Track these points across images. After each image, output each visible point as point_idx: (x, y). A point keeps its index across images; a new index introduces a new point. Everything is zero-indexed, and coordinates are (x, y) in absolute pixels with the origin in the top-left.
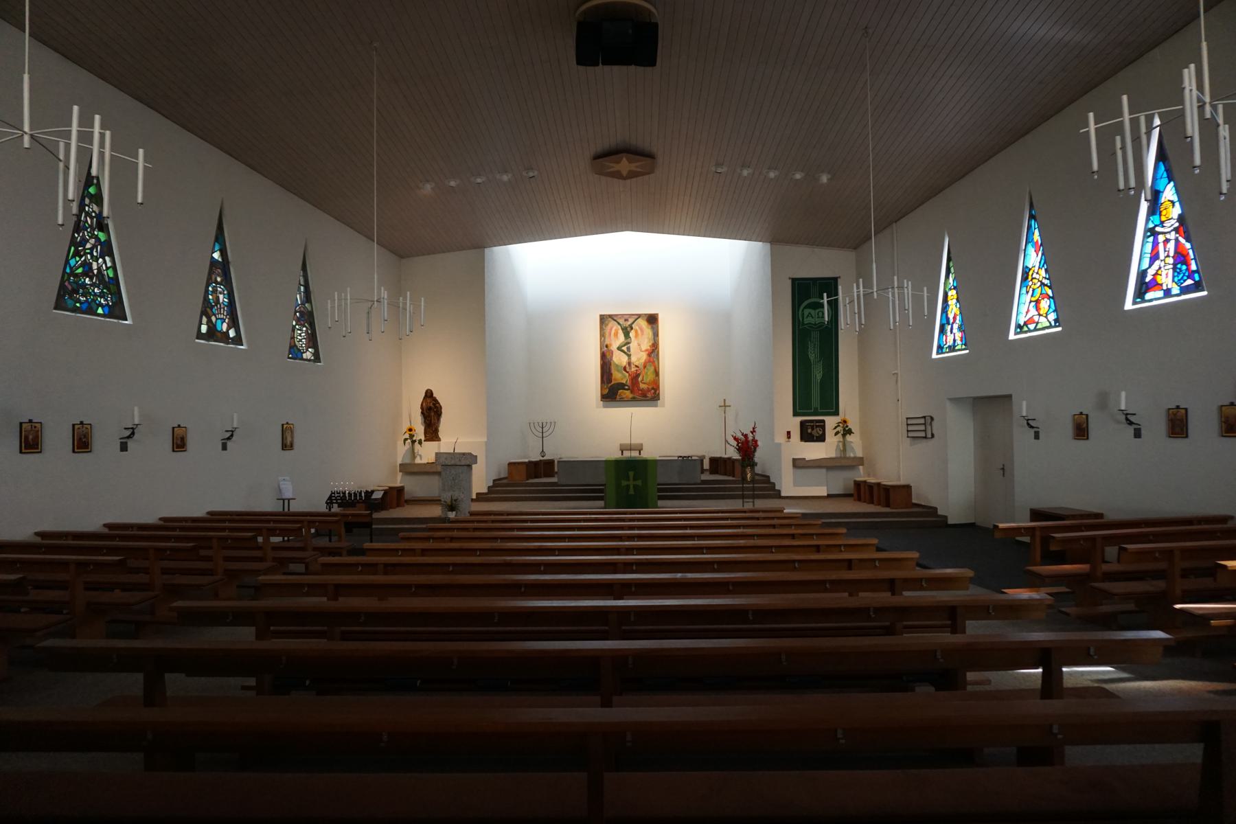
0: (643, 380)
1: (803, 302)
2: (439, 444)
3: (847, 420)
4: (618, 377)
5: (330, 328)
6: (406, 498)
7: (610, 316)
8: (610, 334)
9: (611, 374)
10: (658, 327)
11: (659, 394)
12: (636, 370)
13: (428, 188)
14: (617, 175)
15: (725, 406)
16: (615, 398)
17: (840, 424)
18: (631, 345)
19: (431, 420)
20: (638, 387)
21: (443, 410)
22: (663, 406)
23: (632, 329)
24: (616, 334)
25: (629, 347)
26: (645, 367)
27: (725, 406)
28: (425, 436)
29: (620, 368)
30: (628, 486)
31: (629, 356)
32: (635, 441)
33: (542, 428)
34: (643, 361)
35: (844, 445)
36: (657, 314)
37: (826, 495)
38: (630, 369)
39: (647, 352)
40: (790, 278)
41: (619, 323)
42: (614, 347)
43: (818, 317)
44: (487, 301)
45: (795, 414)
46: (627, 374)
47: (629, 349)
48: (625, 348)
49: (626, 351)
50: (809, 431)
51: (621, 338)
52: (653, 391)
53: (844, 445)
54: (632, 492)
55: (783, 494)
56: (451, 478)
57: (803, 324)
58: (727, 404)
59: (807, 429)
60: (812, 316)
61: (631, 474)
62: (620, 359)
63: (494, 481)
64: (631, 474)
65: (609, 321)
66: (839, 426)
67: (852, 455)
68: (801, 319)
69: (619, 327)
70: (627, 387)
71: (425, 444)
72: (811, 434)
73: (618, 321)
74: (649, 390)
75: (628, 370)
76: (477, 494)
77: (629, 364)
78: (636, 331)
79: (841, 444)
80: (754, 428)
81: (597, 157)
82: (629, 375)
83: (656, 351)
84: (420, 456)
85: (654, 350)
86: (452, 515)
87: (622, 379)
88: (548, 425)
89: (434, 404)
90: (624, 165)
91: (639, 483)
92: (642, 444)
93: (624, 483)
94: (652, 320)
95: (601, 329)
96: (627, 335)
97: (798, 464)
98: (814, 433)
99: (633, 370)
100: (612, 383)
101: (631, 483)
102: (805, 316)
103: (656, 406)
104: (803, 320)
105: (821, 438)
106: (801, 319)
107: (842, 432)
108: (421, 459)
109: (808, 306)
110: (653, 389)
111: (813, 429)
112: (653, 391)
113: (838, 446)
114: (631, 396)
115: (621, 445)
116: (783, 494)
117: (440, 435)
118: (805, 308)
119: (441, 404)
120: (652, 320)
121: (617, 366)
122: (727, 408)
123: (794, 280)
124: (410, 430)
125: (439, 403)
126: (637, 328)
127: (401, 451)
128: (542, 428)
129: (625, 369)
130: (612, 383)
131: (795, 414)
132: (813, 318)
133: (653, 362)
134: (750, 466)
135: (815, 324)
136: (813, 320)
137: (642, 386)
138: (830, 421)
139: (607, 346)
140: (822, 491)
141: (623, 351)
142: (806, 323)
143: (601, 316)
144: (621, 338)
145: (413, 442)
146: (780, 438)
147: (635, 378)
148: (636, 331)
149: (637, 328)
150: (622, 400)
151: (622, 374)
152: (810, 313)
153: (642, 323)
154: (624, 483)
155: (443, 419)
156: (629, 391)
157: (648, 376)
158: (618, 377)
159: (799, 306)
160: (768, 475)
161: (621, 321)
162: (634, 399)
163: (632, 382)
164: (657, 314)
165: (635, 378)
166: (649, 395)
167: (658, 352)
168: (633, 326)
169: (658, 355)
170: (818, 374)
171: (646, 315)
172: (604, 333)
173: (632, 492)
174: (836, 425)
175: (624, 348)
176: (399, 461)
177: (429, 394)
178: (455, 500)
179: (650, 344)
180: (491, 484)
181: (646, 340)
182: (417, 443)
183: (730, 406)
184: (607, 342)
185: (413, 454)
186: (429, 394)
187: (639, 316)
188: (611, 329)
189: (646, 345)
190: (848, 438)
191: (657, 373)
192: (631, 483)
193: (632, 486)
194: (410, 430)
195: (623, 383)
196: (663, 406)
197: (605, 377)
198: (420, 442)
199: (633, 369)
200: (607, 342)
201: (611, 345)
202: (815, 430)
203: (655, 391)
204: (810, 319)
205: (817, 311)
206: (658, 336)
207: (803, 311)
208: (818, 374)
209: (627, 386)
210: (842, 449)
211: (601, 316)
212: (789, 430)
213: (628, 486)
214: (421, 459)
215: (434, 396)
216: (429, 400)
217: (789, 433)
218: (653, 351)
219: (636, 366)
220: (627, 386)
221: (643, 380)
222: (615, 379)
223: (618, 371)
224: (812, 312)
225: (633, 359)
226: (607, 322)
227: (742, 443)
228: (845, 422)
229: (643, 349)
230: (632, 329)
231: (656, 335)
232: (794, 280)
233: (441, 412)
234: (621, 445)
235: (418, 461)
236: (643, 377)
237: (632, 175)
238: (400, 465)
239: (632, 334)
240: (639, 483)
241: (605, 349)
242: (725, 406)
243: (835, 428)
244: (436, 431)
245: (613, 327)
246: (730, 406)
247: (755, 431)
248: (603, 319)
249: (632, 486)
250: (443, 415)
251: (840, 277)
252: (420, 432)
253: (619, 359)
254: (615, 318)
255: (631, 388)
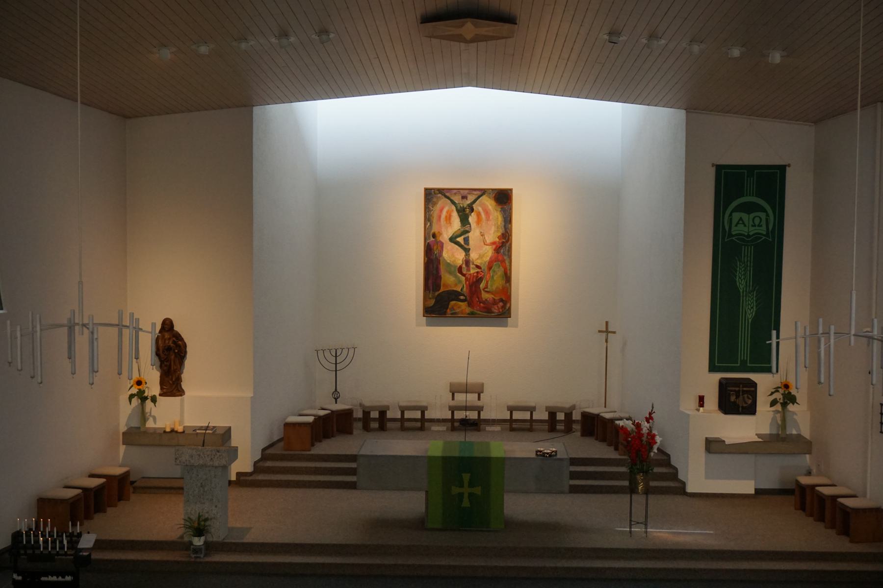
0: (486, 287)
1: (731, 203)
2: (182, 402)
3: (790, 385)
4: (450, 281)
5: (10, 363)
6: (131, 480)
7: (441, 191)
8: (440, 217)
9: (440, 277)
10: (511, 209)
11: (510, 308)
12: (477, 272)
13: (167, 54)
14: (460, 39)
15: (607, 331)
16: (445, 313)
17: (780, 390)
18: (470, 235)
19: (170, 365)
20: (479, 297)
21: (188, 349)
22: (516, 326)
23: (472, 210)
24: (449, 218)
25: (468, 237)
26: (490, 268)
27: (607, 331)
28: (162, 388)
29: (453, 269)
30: (461, 495)
31: (467, 251)
32: (473, 379)
33: (336, 356)
34: (487, 259)
35: (784, 420)
36: (511, 190)
37: (752, 491)
38: (469, 270)
39: (494, 246)
40: (713, 165)
41: (453, 202)
42: (445, 236)
43: (754, 226)
44: (256, 197)
45: (713, 368)
46: (463, 278)
47: (466, 240)
48: (461, 240)
49: (462, 243)
50: (733, 398)
51: (456, 224)
52: (501, 304)
53: (784, 420)
54: (466, 503)
55: (690, 489)
56: (199, 485)
57: (730, 235)
58: (610, 330)
59: (729, 395)
60: (743, 223)
61: (466, 477)
62: (453, 255)
63: (264, 450)
64: (466, 477)
65: (438, 199)
66: (778, 391)
67: (794, 432)
68: (727, 228)
69: (454, 208)
70: (462, 297)
71: (163, 401)
72: (734, 402)
73: (452, 198)
74: (495, 302)
75: (464, 272)
76: (239, 474)
77: (467, 262)
78: (479, 215)
79: (778, 416)
80: (650, 414)
81: (427, 19)
82: (467, 279)
83: (508, 245)
84: (155, 419)
85: (504, 245)
86: (198, 542)
87: (456, 285)
88: (345, 352)
89: (174, 342)
90: (469, 28)
91: (478, 491)
92: (482, 385)
93: (455, 490)
94: (503, 198)
95: (427, 210)
96: (464, 220)
97: (713, 446)
98: (740, 401)
99: (472, 271)
100: (442, 290)
101: (466, 490)
102: (733, 225)
103: (505, 325)
104: (730, 228)
105: (751, 410)
106: (727, 228)
107: (781, 401)
108: (155, 423)
109: (736, 210)
110: (501, 300)
111: (737, 397)
112: (501, 304)
113: (774, 419)
114: (468, 310)
115: (451, 385)
116: (690, 489)
117: (184, 385)
118: (736, 210)
119: (186, 340)
120: (503, 198)
121: (448, 265)
122: (610, 335)
123: (719, 168)
124: (139, 383)
125: (182, 340)
126: (480, 209)
127: (126, 411)
128: (336, 356)
129: (460, 269)
130: (442, 290)
131: (713, 368)
132: (745, 226)
133: (503, 261)
134: (643, 472)
135: (749, 236)
136: (746, 229)
137: (485, 296)
138: (764, 382)
139: (434, 236)
140: (747, 487)
141: (458, 243)
142: (734, 233)
143: (426, 189)
144: (456, 224)
145: (143, 399)
146: (688, 405)
147: (475, 283)
148: (479, 215)
149: (480, 209)
150: (454, 315)
151: (456, 276)
152: (741, 219)
153: (488, 202)
154: (455, 490)
155: (189, 363)
156: (466, 303)
157: (495, 282)
158: (450, 281)
159: (725, 208)
160: (669, 453)
161: (457, 199)
162: (472, 315)
163: (471, 289)
164: (511, 190)
165: (475, 283)
166: (495, 309)
167: (511, 245)
168: (474, 206)
169: (510, 250)
170: (749, 310)
171: (493, 190)
172: (430, 216)
173: (466, 503)
174: (773, 390)
175: (460, 240)
176: (123, 428)
177: (168, 326)
178: (206, 520)
179: (499, 234)
180: (259, 457)
181: (493, 229)
182: (149, 402)
183: (614, 332)
184: (435, 229)
185: (144, 417)
186: (168, 326)
187: (483, 192)
188: (441, 210)
189: (493, 235)
190: (791, 407)
191: (507, 278)
192: (466, 490)
193: (466, 496)
194: (139, 383)
195: (456, 291)
196: (516, 326)
197: (430, 282)
198: (154, 399)
199: (473, 271)
200: (435, 229)
201: (440, 234)
202: (741, 397)
203: (505, 304)
204: (741, 227)
205: (752, 215)
206: (510, 222)
207: (731, 215)
208: (749, 310)
209: (464, 295)
210: (780, 422)
211: (426, 189)
212: (701, 394)
213: (461, 495)
214: (155, 423)
215: (176, 328)
216: (167, 335)
217: (701, 399)
218: (503, 245)
219: (478, 267)
220: (464, 295)
221: (486, 287)
222: (445, 285)
223: (450, 273)
224: (745, 216)
225: (473, 256)
226: (435, 200)
227: (633, 438)
228: (787, 386)
229: (488, 241)
230: (472, 210)
231: (508, 220)
232: (719, 168)
233: (186, 352)
234: (451, 385)
235: (150, 424)
236: (487, 282)
237: (476, 39)
238: (123, 433)
239: (472, 219)
240: (478, 491)
241: (432, 239)
242: (607, 331)
243: (772, 393)
244: (179, 380)
245: (445, 207)
246: (614, 332)
247: (651, 418)
248: (431, 195)
249: (466, 496)
250: (188, 356)
251: (789, 165)
252: (153, 388)
253: (452, 255)
254: (447, 194)
255: (468, 298)
